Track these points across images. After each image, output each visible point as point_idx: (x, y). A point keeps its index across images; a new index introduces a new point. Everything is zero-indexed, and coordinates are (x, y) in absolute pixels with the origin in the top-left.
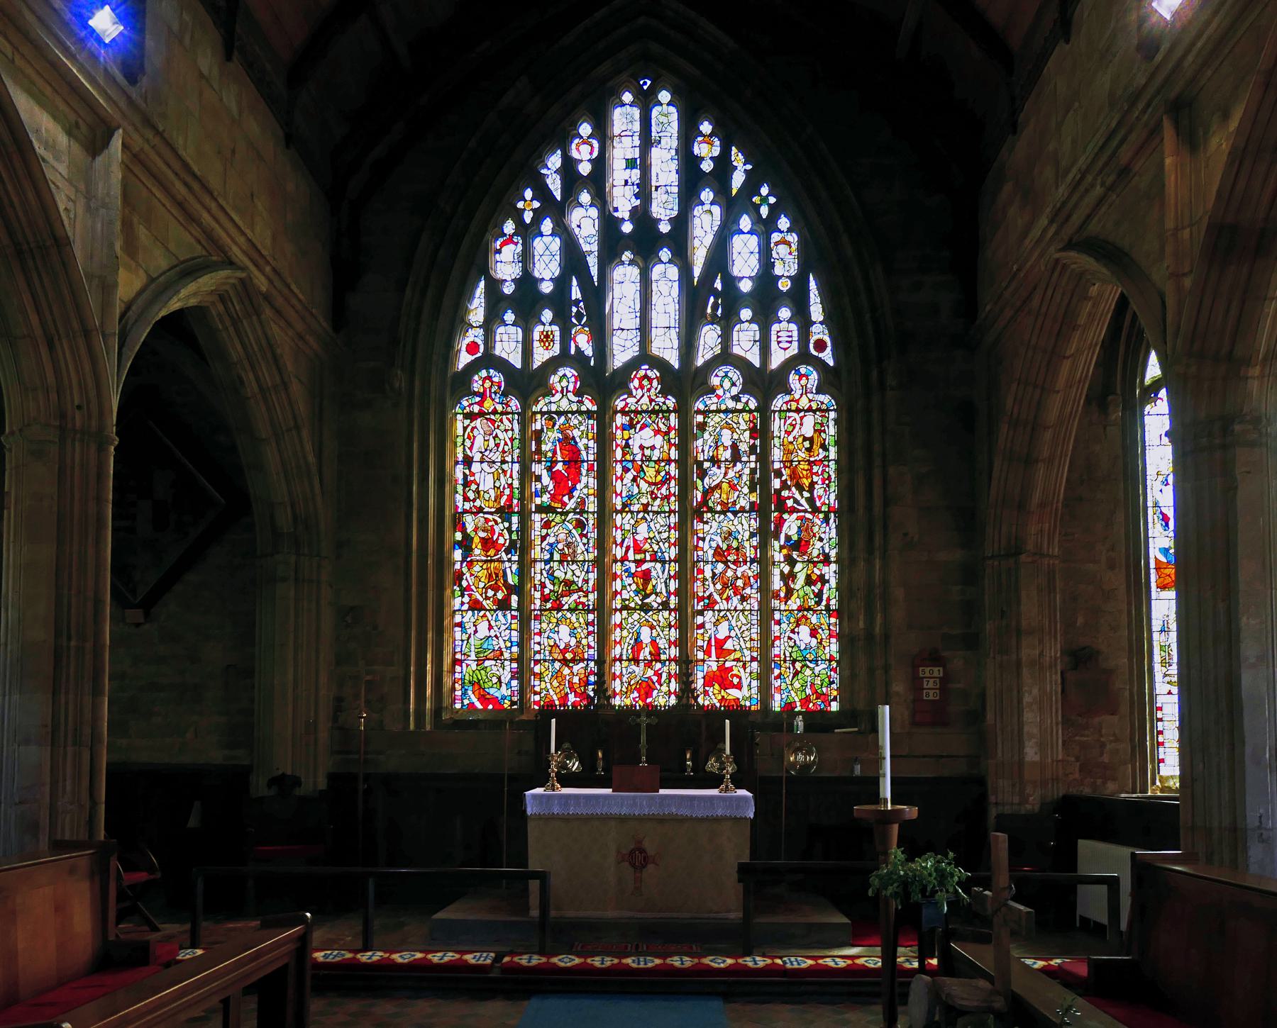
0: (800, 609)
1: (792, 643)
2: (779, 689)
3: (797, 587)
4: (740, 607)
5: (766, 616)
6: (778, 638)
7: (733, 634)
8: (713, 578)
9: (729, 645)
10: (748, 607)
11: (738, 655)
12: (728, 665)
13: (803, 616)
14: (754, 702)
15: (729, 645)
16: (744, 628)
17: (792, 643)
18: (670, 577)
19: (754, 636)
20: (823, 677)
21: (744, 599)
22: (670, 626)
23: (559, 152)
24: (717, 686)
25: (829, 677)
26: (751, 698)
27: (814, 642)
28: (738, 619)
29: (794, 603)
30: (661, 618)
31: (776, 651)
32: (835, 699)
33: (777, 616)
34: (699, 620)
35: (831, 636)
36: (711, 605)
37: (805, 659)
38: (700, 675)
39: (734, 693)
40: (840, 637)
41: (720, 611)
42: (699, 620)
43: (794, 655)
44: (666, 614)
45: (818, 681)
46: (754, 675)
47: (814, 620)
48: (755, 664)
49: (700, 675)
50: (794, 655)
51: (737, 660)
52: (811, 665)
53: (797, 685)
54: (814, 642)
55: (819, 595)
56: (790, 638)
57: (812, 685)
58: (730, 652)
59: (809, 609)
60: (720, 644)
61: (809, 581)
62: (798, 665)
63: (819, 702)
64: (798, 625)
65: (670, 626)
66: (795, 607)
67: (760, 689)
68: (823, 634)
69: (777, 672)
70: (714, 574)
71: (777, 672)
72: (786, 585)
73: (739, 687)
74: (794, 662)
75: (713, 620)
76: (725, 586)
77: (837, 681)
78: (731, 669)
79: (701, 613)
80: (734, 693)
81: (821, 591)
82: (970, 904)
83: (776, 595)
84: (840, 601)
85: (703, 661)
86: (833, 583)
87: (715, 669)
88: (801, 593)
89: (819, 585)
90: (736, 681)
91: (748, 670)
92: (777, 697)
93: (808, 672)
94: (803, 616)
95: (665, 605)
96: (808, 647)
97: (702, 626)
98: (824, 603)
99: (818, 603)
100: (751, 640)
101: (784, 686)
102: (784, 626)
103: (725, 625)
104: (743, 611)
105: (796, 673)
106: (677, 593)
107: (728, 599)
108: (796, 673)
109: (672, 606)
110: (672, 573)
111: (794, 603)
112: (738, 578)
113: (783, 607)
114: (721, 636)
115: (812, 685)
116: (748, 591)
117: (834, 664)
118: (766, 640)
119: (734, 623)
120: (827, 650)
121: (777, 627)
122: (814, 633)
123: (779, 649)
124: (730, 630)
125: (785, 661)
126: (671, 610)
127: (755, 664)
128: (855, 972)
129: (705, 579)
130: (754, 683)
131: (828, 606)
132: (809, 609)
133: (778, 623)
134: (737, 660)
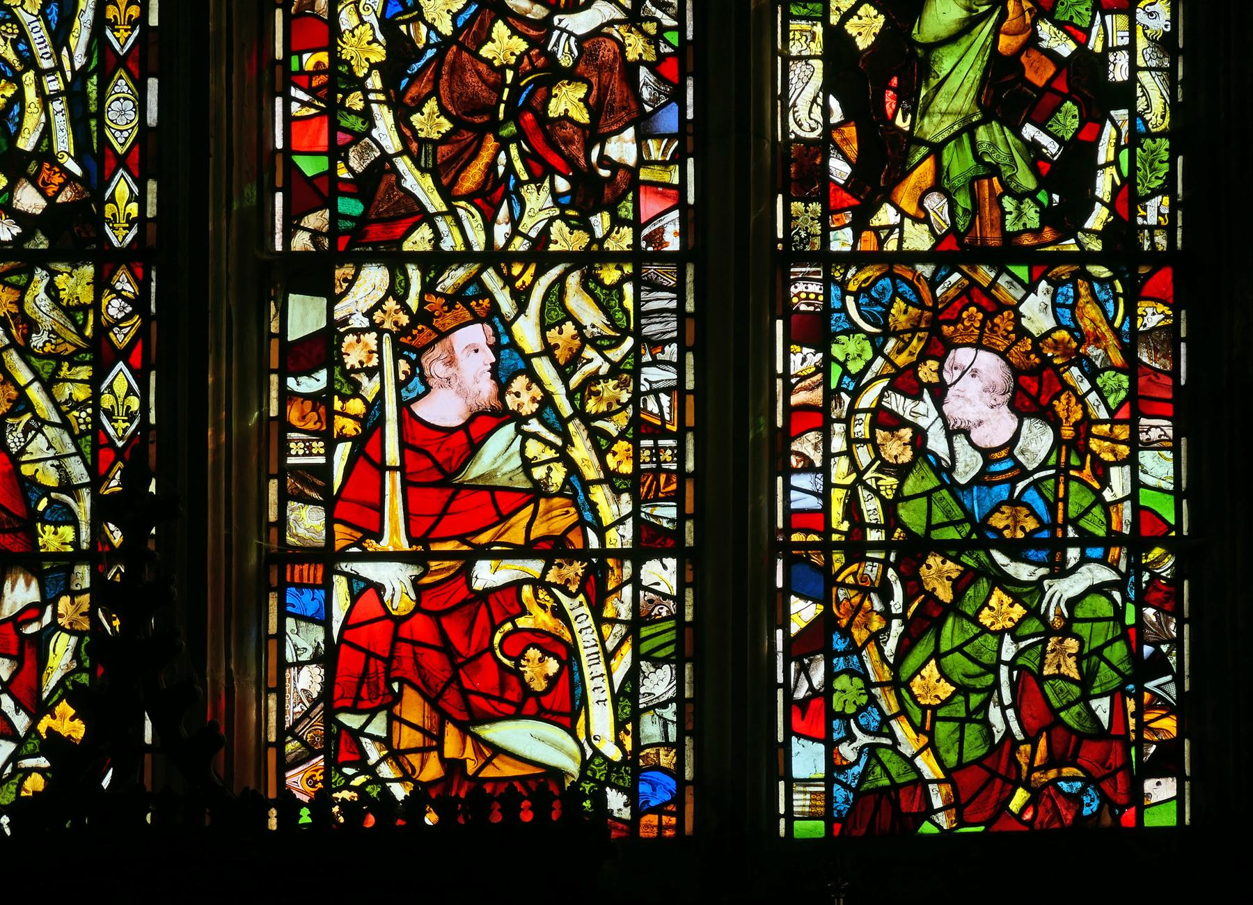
0: (953, 251)
1: (897, 449)
2: (821, 717)
3: (934, 128)
4: (565, 239)
5: (734, 291)
6: (819, 419)
7: (522, 397)
8: (391, 70)
9: (497, 457)
10: (623, 240)
11: (556, 519)
12: (486, 575)
13: (970, 292)
14: (658, 791)
15: (497, 457)
16: (595, 362)
17: (897, 449)
18: (104, 61)
19: (660, 407)
20: (1098, 635)
21: (591, 193)
22: (101, 355)
23: (793, 597)
24: (413, 708)
25: (1135, 636)
26: (631, 770)
27: (1037, 442)
28: (555, 312)
29: (911, 224)
30: (38, 299)
31: (802, 493)
32: (1165, 764)
33: (805, 291)
34: (304, 316)
35: (1137, 406)
36: (378, 226)
37: (982, 536)
38: (303, 640)
39: (531, 741)
40: (1189, 414)
41: (435, 261)
42: (304, 316)
43: (913, 516)
44: (77, 283)
45: (1063, 661)
46: (659, 636)
47: (1037, 313)
48: (661, 574)
49: (303, 640)
50: (913, 516)
51: (552, 549)
52: (1023, 572)
53: (930, 685)
54: (1037, 442)
55: (1070, 175)
56: (884, 419)
57: (1028, 681)
58: (500, 501)
59: (1007, 252)
60: (439, 460)
61: (1006, 93)
62: (938, 575)
63: (1070, 779)
64: (939, 348)
65: (101, 355)
66: (918, 239)
67: (692, 712)
68: (1098, 396)
69: (803, 612)
70: (400, 51)
71: (803, 612)
72: (864, 112)
73: (563, 705)
74: (911, 552)
75: (394, 317)
76: (472, 122)
77: (1181, 658)
78: (507, 599)
79: (315, 275)
80: (531, 741)
81: (1080, 154)
82: (276, 151)
83: (802, 169)
84: (1193, 206)
85: (327, 558)
86: (1154, 97)
87: (400, 597)
88: (959, 163)
89: (1069, 118)
90: (539, 669)
91: (620, 606)
92: (807, 759)
93: (1002, 610)
94: (970, 292)
95: (72, 232)
96: (1000, 464)
97: (323, 348)
98: (1098, 218)
99: (1066, 218)
100: (639, 428)
101: (847, 692)
102: (851, 350)
103: (469, 351)
104: (587, 261)
105: (926, 619)
106: (148, 156)
107: (494, 195)
108: (926, 619)
109: (120, 237)
110: (121, 40)
111: (911, 224)
112: (554, 74)
113: (842, 241)
114: (442, 410)
115: (1028, 681)
116: (622, 148)
117: (1162, 562)
118: (734, 435)
119: (527, 333)
120: (1119, 480)
121: (804, 360)
122: (1031, 393)
123: (822, 480)
124: (501, 378)
125: (856, 548)
126: (107, 262)
127: (661, 574)
128: (814, 542)
129: (340, 78)
130: (659, 683)
131: (1122, 233)
132: (1007, 252)
133: (817, 331)
134: (552, 549)
